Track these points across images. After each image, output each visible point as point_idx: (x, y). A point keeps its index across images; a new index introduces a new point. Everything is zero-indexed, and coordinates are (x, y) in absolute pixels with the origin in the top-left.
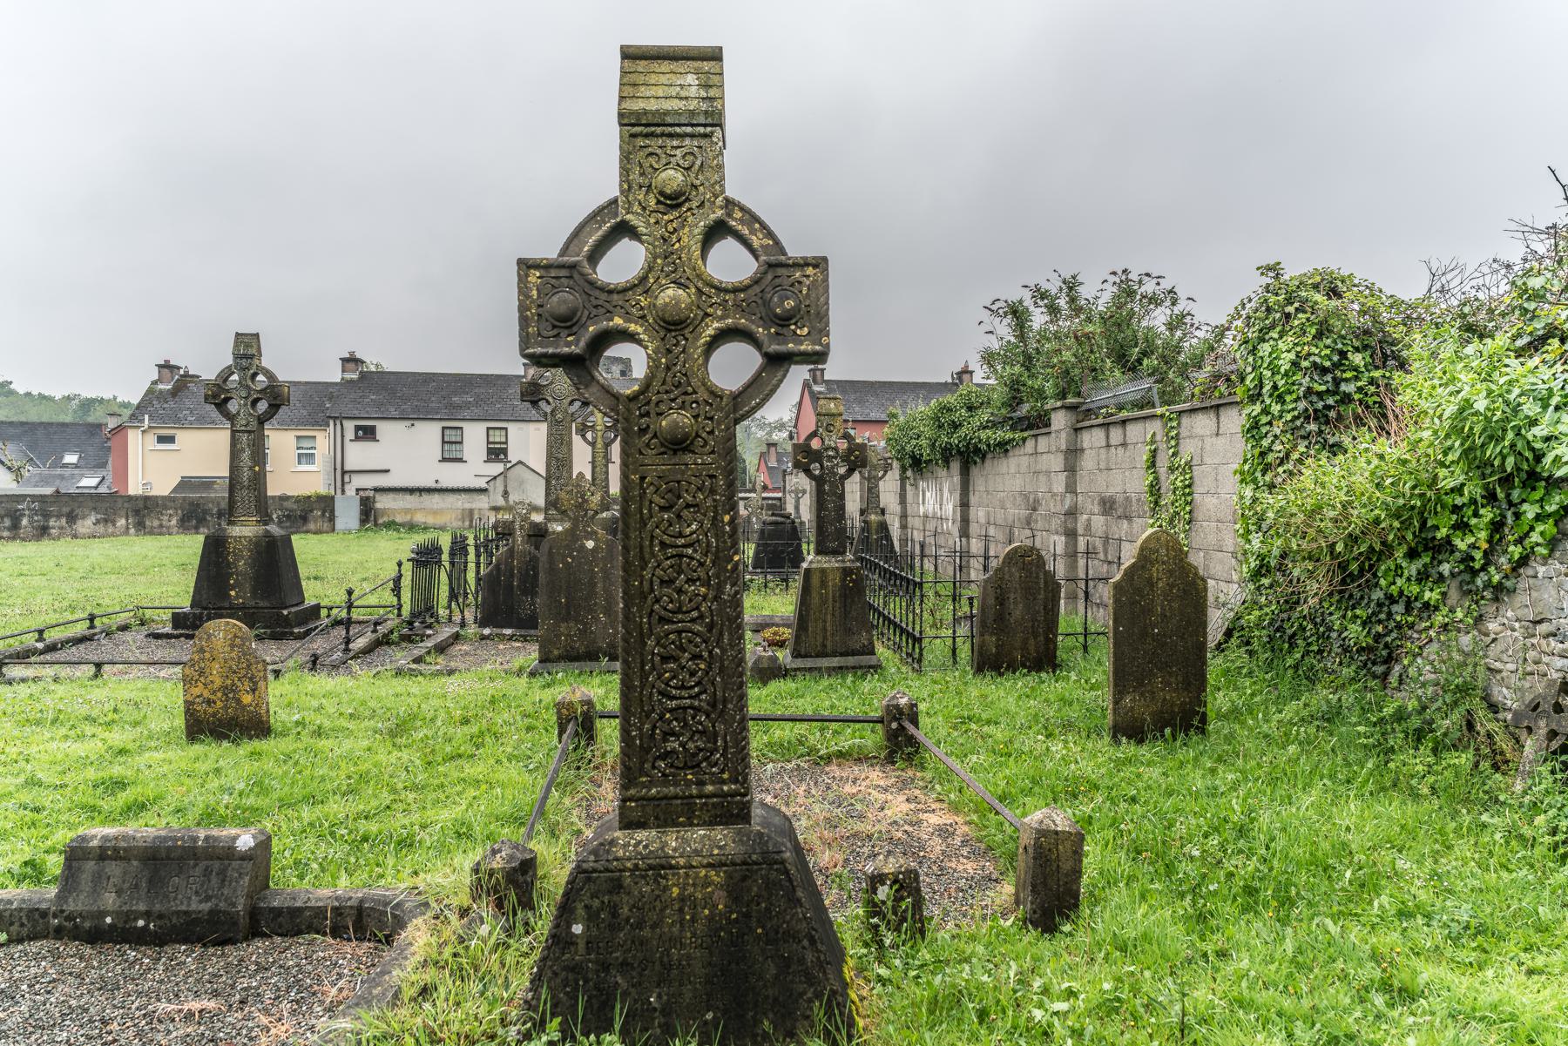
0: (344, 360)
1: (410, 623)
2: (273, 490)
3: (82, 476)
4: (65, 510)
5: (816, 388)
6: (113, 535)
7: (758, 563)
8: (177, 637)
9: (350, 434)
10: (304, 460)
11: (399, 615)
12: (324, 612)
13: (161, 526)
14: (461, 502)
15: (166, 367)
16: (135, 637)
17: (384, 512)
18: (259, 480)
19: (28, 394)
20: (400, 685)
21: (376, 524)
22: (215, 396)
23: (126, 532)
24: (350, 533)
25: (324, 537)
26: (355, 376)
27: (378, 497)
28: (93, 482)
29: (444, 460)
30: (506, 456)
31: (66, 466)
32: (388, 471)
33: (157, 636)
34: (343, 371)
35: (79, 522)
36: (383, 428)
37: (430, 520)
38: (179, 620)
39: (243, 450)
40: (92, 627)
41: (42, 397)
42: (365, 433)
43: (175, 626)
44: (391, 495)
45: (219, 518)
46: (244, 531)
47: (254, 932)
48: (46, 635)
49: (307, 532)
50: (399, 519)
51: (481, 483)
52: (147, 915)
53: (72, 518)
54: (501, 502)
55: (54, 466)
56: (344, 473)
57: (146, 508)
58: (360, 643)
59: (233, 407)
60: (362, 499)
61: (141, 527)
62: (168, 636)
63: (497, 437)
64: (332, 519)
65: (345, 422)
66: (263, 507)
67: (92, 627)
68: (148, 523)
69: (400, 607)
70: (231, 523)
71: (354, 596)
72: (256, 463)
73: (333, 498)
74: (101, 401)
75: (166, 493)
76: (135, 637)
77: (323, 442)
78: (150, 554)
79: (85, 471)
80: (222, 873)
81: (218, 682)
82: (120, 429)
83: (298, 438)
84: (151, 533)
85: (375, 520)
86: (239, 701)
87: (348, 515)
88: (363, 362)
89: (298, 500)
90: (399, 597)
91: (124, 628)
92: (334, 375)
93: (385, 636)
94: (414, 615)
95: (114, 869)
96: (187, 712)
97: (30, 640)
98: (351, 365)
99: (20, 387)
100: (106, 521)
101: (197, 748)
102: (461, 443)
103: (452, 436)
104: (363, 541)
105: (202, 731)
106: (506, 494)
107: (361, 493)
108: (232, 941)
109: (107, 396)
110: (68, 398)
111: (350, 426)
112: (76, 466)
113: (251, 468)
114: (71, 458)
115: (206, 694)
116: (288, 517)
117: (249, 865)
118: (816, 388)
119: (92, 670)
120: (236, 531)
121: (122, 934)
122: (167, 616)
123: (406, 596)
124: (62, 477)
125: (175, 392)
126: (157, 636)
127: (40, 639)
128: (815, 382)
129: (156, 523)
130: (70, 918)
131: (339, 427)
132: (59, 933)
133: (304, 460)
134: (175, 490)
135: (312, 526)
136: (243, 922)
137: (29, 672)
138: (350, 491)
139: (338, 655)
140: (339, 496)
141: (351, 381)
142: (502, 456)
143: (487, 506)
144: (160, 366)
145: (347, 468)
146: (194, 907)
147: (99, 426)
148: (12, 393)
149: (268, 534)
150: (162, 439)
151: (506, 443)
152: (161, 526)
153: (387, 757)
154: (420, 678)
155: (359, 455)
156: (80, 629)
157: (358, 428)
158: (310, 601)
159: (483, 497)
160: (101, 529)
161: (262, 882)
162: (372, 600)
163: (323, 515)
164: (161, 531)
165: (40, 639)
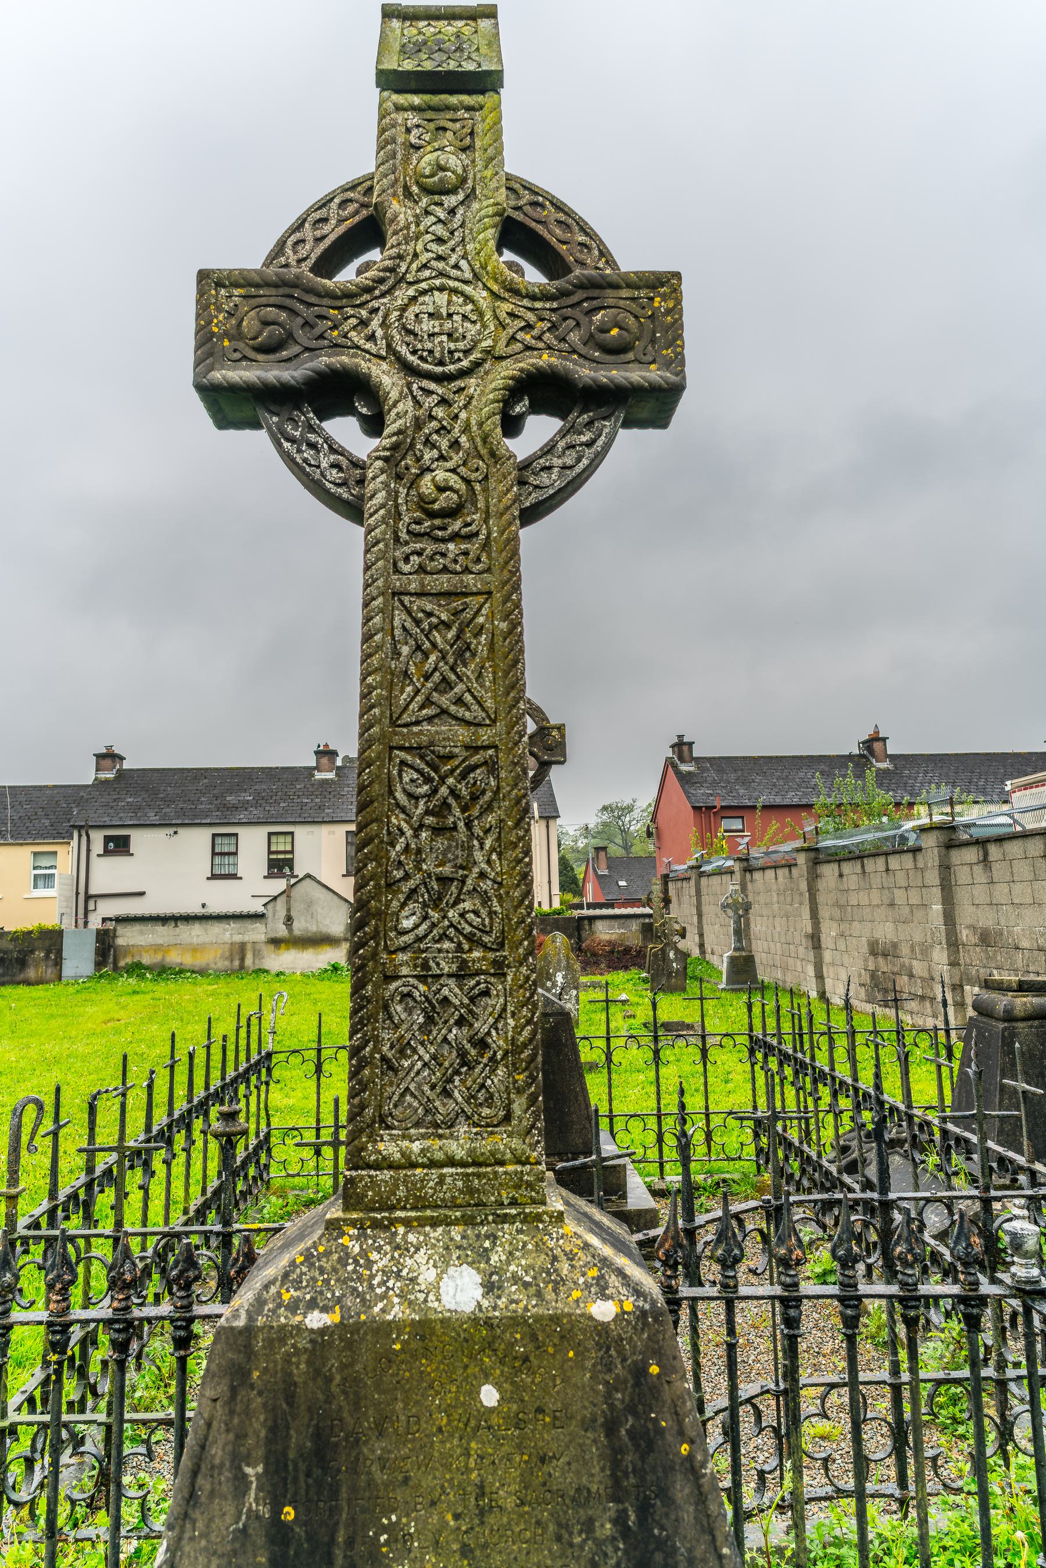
0: (99, 757)
5: (684, 768)
9: (98, 847)
10: (40, 883)
14: (228, 934)
17: (127, 950)
26: (110, 775)
27: (121, 930)
29: (214, 877)
30: (292, 869)
32: (142, 894)
34: (97, 770)
37: (188, 960)
44: (137, 927)
51: (257, 907)
54: (282, 931)
56: (88, 897)
63: (281, 845)
64: (58, 963)
83: (35, 854)
92: (86, 775)
98: (107, 762)
102: (235, 854)
103: (225, 846)
106: (289, 920)
111: (98, 838)
118: (684, 768)
128: (682, 759)
133: (40, 883)
135: (31, 973)
141: (106, 782)
142: (287, 870)
143: (263, 938)
145: (92, 891)
151: (292, 852)
157: (107, 839)
159: (259, 926)
163: (47, 956)
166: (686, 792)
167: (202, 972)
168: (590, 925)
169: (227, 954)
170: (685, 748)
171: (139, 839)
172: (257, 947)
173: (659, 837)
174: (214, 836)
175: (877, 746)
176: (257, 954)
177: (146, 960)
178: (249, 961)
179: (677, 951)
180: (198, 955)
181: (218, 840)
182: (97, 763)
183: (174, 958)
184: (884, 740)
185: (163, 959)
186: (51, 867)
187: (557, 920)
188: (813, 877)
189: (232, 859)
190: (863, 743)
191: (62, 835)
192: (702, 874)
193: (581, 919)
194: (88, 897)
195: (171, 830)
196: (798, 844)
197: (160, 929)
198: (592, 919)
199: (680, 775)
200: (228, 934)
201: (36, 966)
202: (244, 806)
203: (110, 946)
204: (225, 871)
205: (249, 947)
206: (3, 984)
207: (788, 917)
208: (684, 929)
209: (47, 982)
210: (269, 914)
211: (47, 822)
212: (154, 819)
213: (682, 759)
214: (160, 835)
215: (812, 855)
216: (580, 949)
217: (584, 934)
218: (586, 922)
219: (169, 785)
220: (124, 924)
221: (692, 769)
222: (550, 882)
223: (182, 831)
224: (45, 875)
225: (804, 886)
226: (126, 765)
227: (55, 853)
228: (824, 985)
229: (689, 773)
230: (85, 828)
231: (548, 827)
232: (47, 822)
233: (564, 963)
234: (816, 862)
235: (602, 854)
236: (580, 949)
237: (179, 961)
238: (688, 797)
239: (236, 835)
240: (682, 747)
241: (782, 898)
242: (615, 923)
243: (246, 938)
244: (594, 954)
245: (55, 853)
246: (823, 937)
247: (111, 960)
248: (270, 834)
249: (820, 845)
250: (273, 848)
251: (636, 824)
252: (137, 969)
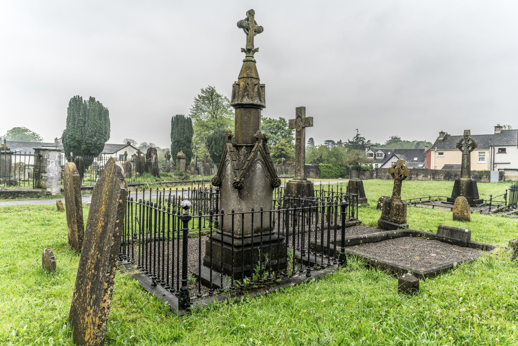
0: (496, 127)
1: (509, 207)
2: (472, 169)
3: (419, 164)
4: (416, 173)
6: (427, 180)
7: (335, 147)
8: (448, 203)
10: (481, 160)
11: (506, 205)
12: (484, 202)
13: (439, 178)
15: (442, 133)
16: (439, 203)
17: (507, 177)
18: (469, 167)
19: (404, 141)
20: (502, 218)
21: (504, 181)
22: (459, 146)
23: (430, 180)
24: (495, 183)
25: (487, 184)
26: (499, 132)
27: (506, 172)
28: (422, 165)
31: (414, 161)
32: (510, 163)
33: (444, 203)
34: (495, 131)
35: (419, 176)
36: (508, 149)
38: (448, 200)
39: (465, 159)
40: (430, 199)
41: (408, 142)
42: (502, 151)
43: (448, 201)
44: (510, 171)
45: (455, 177)
46: (465, 179)
47: (467, 246)
48: (422, 200)
49: (481, 182)
50: (513, 180)
52: (450, 239)
53: (417, 175)
55: (412, 161)
56: (494, 164)
57: (435, 173)
58: (493, 210)
59: (463, 148)
60: (500, 172)
61: (434, 178)
62: (446, 203)
64: (489, 178)
65: (495, 148)
66: (469, 173)
67: (430, 199)
68: (436, 177)
69: (506, 203)
70: (461, 177)
71: (492, 197)
72: (468, 162)
73: (490, 172)
74: (422, 142)
75: (440, 169)
76: (439, 203)
77: (487, 154)
78: (438, 185)
79: (420, 163)
80: (463, 235)
81: (460, 209)
82: (429, 151)
83: (479, 152)
84: (436, 180)
85: (504, 180)
86: (464, 214)
87: (495, 176)
88: (502, 127)
89: (479, 172)
90: (506, 199)
91: (436, 200)
92: (492, 132)
93: (501, 209)
94: (509, 204)
95: (445, 231)
96: (453, 215)
97: (418, 200)
98: (498, 129)
99: (402, 139)
100: (425, 176)
101: (455, 222)
104: (499, 186)
105: (456, 219)
107: (500, 170)
108: (464, 247)
109: (423, 140)
110: (414, 142)
111: (497, 149)
112: (417, 161)
113: (467, 164)
114: (416, 159)
115: (457, 212)
116: (475, 177)
117: (467, 235)
119: (432, 207)
120: (463, 179)
121: (445, 241)
122: (446, 198)
123: (508, 201)
124: (414, 164)
125: (443, 140)
126: (444, 203)
127: (420, 200)
129: (438, 177)
130: (439, 237)
131: (493, 149)
132: (437, 239)
133: (481, 160)
134: (443, 168)
135: (483, 180)
136: (466, 244)
137: (420, 206)
138: (496, 169)
139: (487, 212)
140: (492, 171)
141: (498, 134)
144: (440, 133)
145: (495, 162)
146: (458, 239)
147: (423, 150)
148: (401, 141)
149: (470, 180)
150: (440, 154)
152: (439, 178)
153: (496, 229)
154: (508, 218)
155: (499, 158)
156: (427, 199)
157: (499, 149)
158: (481, 198)
160: (424, 178)
161: (469, 238)
162: (497, 200)
163: (486, 177)
164: (439, 180)
165: (420, 200)
191: (487, 148)
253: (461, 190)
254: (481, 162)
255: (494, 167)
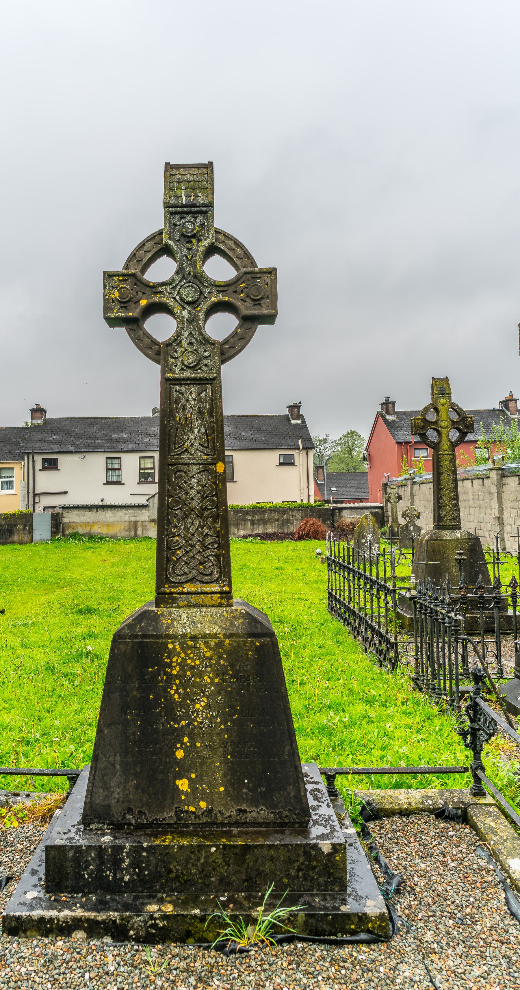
0: (33, 410)
9: (39, 465)
10: (5, 486)
14: (127, 516)
17: (70, 525)
26: (40, 422)
27: (65, 513)
29: (107, 483)
32: (66, 493)
34: (32, 419)
37: (105, 531)
39: (188, 425)
44: (75, 512)
56: (35, 495)
64: (31, 532)
85: (63, 532)
98: (38, 414)
111: (39, 459)
118: (390, 418)
128: (388, 412)
133: (5, 486)
135: (16, 538)
138: (39, 509)
141: (38, 426)
143: (147, 519)
145: (37, 491)
157: (44, 460)
159: (145, 511)
163: (24, 528)
166: (392, 433)
167: (114, 537)
168: (340, 513)
169: (127, 528)
170: (390, 406)
171: (64, 460)
172: (144, 524)
173: (370, 460)
174: (107, 459)
175: (511, 404)
176: (144, 528)
177: (81, 531)
178: (139, 532)
179: (415, 526)
180: (110, 528)
181: (110, 461)
182: (32, 415)
183: (96, 530)
184: (516, 400)
185: (90, 531)
186: (10, 477)
187: (319, 510)
188: (501, 485)
189: (118, 473)
190: (502, 402)
192: (414, 483)
193: (334, 509)
194: (35, 495)
195: (81, 455)
196: (490, 465)
197: (88, 513)
198: (340, 509)
199: (386, 421)
200: (127, 517)
201: (18, 534)
202: (123, 441)
203: (60, 523)
204: (114, 480)
205: (139, 524)
206: (3, 544)
207: (480, 508)
208: (419, 513)
209: (25, 543)
210: (151, 505)
211: (6, 450)
212: (72, 449)
213: (388, 412)
214: (76, 458)
215: (500, 472)
216: (333, 527)
217: (336, 518)
218: (337, 511)
219: (76, 428)
220: (67, 510)
221: (394, 419)
222: (308, 487)
223: (88, 456)
224: (7, 482)
225: (494, 490)
226: (48, 416)
227: (13, 469)
228: (505, 544)
229: (393, 421)
230: (32, 454)
231: (307, 454)
232: (6, 450)
233: (372, 530)
234: (503, 476)
235: (321, 470)
236: (333, 527)
237: (99, 531)
238: (393, 436)
239: (120, 458)
240: (388, 405)
241: (476, 497)
242: (354, 512)
243: (137, 519)
244: (343, 530)
245: (13, 469)
246: (505, 518)
247: (61, 530)
248: (140, 458)
249: (505, 467)
250: (142, 466)
251: (361, 451)
252: (75, 536)
253: (178, 735)
254: (6, 492)
255: (34, 503)
